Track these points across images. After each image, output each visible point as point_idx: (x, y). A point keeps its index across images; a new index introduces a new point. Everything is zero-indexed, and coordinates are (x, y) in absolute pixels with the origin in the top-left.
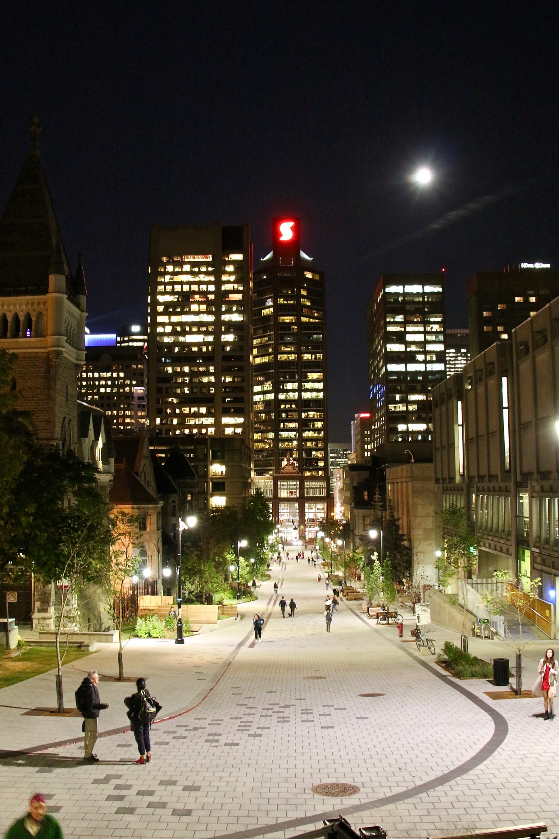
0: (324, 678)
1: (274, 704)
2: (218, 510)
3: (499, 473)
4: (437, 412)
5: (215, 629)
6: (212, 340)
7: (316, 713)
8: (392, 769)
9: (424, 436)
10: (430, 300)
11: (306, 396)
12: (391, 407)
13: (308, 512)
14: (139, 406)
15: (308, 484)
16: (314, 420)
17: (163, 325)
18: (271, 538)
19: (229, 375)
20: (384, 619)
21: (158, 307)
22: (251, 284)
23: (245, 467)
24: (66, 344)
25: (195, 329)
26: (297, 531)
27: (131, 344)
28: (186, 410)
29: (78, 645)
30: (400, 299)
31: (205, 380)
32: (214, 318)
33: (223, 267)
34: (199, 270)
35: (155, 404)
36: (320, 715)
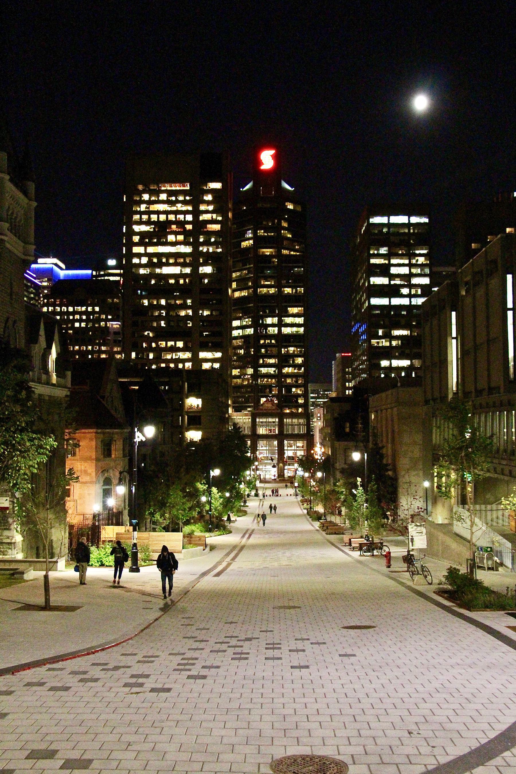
2: (192, 443)
3: (502, 383)
6: (189, 272)
7: (285, 648)
8: (398, 733)
10: (416, 231)
11: (286, 330)
12: (374, 342)
13: (287, 450)
14: (115, 341)
16: (294, 356)
17: (139, 256)
18: (248, 474)
19: (207, 309)
20: (368, 550)
21: (134, 237)
22: (230, 215)
24: (8, 233)
25: (171, 261)
26: (275, 469)
27: (106, 278)
28: (163, 344)
29: (12, 572)
30: (385, 230)
31: (183, 313)
32: (192, 249)
33: (201, 196)
34: (176, 199)
36: (290, 651)
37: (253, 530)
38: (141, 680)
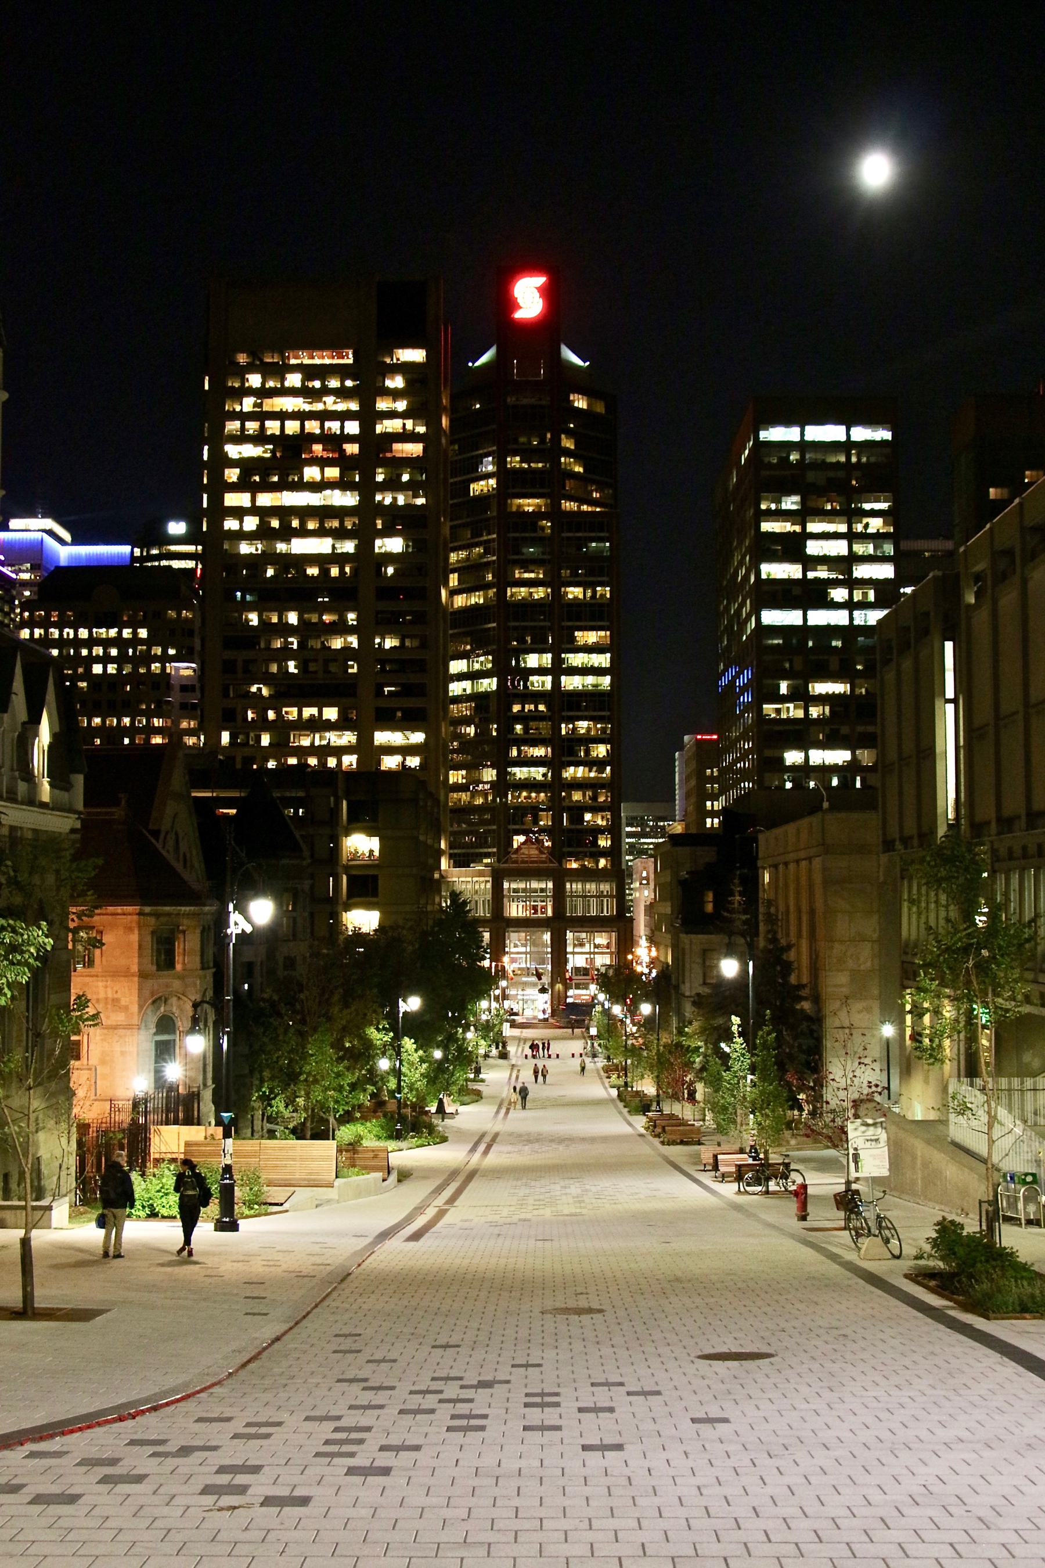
0: (600, 1311)
1: (448, 1379)
2: (359, 937)
4: (890, 676)
5: (329, 1201)
7: (569, 1406)
9: (845, 777)
11: (571, 683)
12: (769, 708)
15: (573, 887)
16: (589, 740)
17: (239, 513)
18: (485, 1008)
19: (392, 633)
21: (227, 471)
22: (445, 422)
25: (311, 525)
26: (547, 997)
27: (164, 563)
30: (794, 457)
31: (337, 643)
32: (358, 498)
35: (219, 698)
36: (581, 1410)
37: (496, 1135)
38: (241, 1479)
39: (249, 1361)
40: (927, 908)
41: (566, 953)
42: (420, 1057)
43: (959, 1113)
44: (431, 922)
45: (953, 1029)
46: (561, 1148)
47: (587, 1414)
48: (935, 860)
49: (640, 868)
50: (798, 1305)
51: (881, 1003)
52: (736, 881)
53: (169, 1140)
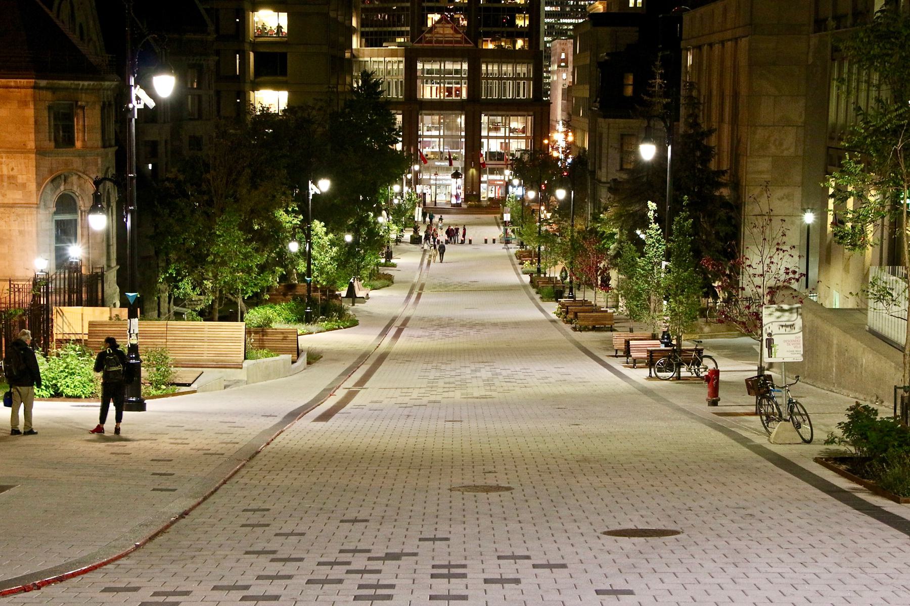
0: (508, 489)
2: (266, 116)
5: (237, 382)
7: (475, 576)
15: (489, 68)
20: (669, 367)
23: (336, 20)
26: (460, 181)
36: (486, 581)
37: (407, 320)
39: (156, 535)
40: (858, 89)
41: (481, 137)
42: (330, 240)
43: (879, 299)
44: (342, 103)
45: (878, 212)
46: (472, 332)
47: (493, 585)
48: (869, 37)
49: (558, 51)
50: (706, 486)
51: (803, 190)
52: (658, 63)
53: (72, 321)
